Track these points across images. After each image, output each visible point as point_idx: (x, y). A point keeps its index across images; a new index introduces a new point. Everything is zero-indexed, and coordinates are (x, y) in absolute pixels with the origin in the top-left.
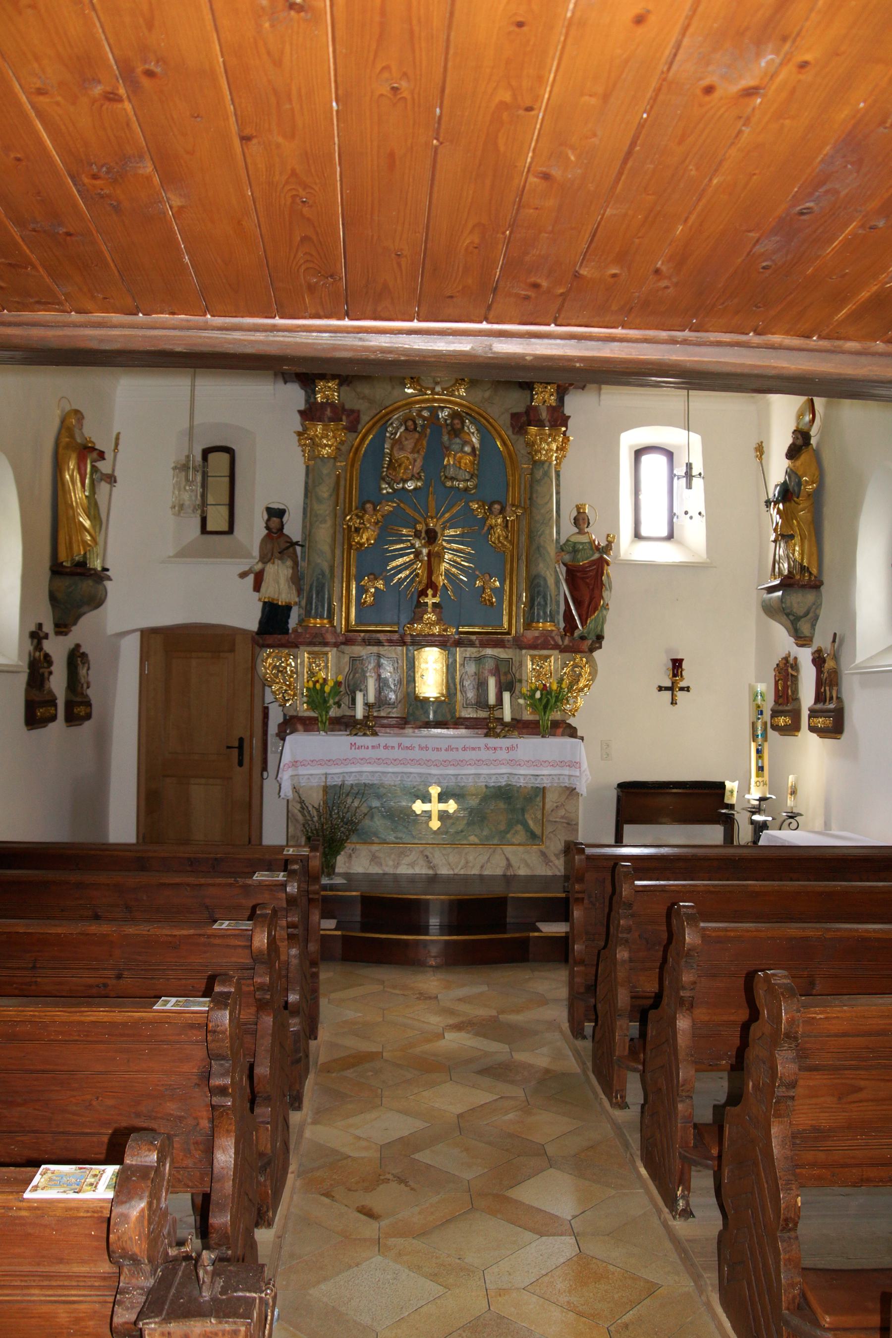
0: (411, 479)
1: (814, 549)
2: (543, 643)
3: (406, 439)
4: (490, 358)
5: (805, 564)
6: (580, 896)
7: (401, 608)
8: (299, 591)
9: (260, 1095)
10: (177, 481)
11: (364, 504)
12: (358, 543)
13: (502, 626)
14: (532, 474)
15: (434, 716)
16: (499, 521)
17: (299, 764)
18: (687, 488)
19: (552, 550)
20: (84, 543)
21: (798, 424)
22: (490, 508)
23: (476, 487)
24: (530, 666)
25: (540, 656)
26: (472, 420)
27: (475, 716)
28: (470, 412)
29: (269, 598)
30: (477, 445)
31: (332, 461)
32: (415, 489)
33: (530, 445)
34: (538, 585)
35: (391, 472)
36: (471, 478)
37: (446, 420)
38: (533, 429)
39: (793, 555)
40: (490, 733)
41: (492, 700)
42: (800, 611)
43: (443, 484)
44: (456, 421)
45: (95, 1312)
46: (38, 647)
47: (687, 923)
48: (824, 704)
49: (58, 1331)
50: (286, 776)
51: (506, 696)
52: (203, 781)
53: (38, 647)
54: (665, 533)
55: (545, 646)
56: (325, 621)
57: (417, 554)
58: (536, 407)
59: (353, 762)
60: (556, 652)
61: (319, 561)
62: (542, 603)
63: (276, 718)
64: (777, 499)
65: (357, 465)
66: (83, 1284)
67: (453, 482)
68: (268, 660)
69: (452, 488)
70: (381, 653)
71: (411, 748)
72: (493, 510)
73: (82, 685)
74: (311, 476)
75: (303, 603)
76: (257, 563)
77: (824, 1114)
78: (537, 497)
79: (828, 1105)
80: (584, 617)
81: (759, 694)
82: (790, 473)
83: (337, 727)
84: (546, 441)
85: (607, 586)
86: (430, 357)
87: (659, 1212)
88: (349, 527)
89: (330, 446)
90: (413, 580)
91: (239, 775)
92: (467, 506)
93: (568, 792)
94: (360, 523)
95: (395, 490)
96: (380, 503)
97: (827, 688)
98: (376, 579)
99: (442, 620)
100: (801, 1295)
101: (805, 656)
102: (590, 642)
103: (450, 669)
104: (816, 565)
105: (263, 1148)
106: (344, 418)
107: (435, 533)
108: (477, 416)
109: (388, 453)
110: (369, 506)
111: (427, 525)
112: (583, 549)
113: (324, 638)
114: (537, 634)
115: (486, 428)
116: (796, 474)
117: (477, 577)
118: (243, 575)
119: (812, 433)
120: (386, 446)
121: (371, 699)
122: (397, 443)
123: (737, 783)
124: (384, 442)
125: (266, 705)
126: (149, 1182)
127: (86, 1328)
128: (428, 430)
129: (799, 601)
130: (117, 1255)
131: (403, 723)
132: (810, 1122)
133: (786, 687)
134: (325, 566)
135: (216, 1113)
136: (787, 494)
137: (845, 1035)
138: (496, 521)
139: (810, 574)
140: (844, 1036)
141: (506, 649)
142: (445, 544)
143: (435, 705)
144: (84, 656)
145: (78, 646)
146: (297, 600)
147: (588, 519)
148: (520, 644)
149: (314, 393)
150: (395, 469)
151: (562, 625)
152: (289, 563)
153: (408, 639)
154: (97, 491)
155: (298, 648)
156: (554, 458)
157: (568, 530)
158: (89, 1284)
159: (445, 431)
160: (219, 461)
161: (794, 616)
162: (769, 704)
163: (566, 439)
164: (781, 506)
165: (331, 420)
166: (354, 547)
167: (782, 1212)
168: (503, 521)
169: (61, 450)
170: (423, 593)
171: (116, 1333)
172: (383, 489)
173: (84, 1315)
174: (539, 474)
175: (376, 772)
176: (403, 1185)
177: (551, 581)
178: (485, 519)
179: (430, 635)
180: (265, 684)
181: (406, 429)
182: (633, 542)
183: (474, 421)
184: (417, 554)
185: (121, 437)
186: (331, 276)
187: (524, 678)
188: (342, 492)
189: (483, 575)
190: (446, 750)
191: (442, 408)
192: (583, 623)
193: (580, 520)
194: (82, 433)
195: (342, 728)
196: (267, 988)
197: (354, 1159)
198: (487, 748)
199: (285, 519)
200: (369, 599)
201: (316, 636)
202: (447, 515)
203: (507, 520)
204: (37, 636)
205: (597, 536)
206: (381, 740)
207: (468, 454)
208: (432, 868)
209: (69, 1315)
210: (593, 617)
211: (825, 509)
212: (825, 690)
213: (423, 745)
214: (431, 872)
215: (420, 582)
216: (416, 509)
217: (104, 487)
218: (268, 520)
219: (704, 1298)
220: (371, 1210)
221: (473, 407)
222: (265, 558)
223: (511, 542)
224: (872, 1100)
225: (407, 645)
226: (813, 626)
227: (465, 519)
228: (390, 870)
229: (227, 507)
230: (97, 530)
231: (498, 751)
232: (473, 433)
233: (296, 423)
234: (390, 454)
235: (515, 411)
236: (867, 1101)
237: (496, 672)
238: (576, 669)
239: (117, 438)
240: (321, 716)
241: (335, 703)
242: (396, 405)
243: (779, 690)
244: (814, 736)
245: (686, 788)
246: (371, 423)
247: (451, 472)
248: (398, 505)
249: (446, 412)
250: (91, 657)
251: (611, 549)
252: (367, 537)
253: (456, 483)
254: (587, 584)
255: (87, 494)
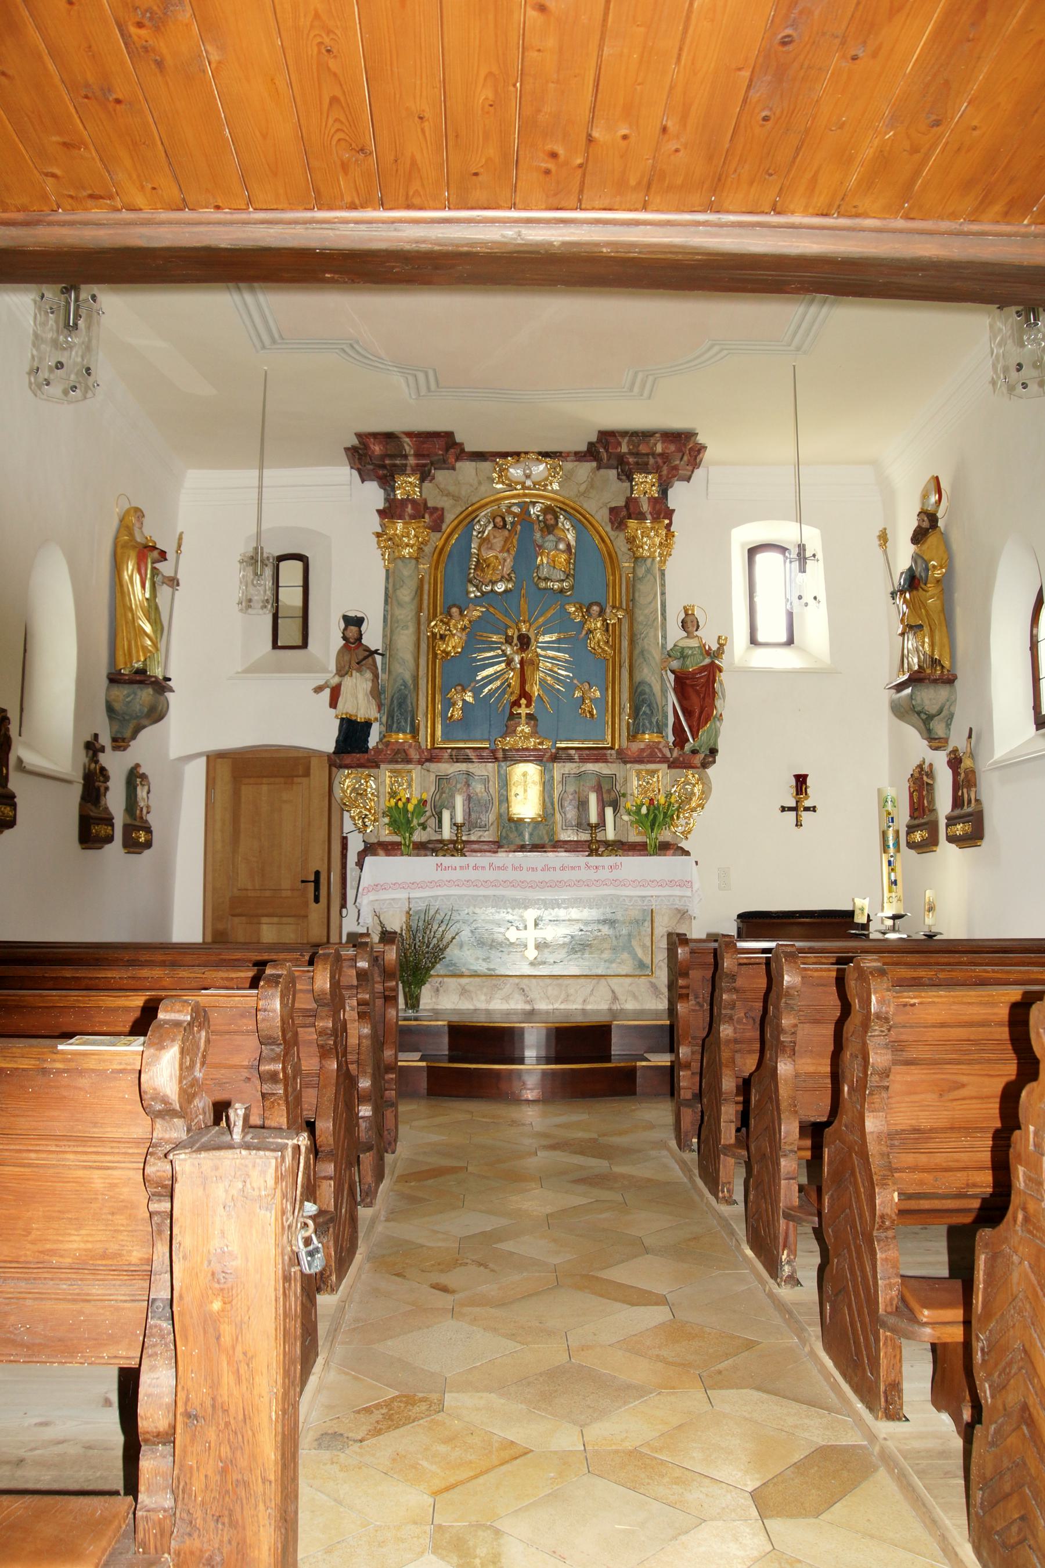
0: (501, 580)
1: (946, 641)
2: (649, 756)
3: (495, 537)
4: (520, 245)
5: (936, 657)
6: (684, 991)
7: (492, 722)
8: (380, 706)
9: (322, 1149)
10: (243, 576)
11: (450, 608)
12: (444, 651)
13: (604, 740)
14: (634, 572)
15: (530, 839)
16: (599, 625)
17: (379, 887)
18: (800, 571)
19: (656, 655)
20: (145, 648)
21: (923, 504)
22: (588, 611)
23: (572, 588)
24: (635, 783)
25: (647, 771)
26: (568, 516)
27: (575, 839)
28: (564, 507)
29: (346, 714)
30: (573, 543)
31: (414, 562)
32: (506, 591)
33: (631, 540)
34: (643, 693)
35: (479, 573)
36: (567, 578)
37: (538, 516)
38: (632, 523)
39: (923, 647)
40: (594, 852)
41: (594, 819)
42: (933, 709)
43: (537, 585)
44: (549, 517)
45: (129, 1179)
46: (94, 759)
47: (786, 960)
48: (962, 809)
49: (93, 1196)
50: (365, 901)
51: (609, 811)
52: (275, 920)
53: (94, 759)
54: (784, 638)
55: (652, 758)
56: (409, 736)
57: (509, 662)
58: (636, 498)
59: (438, 884)
60: (665, 766)
61: (401, 670)
62: (648, 712)
63: (355, 845)
64: (903, 586)
65: (441, 566)
66: (117, 1151)
67: (546, 583)
68: (346, 781)
69: (545, 589)
70: (470, 770)
71: (504, 868)
72: (592, 611)
73: (142, 809)
74: (391, 580)
75: (384, 719)
76: (334, 676)
77: (923, 1113)
78: (639, 597)
79: (927, 1103)
80: (695, 730)
81: (889, 800)
82: (916, 558)
83: (423, 852)
84: (648, 536)
85: (720, 694)
86: (463, 246)
87: (763, 1282)
88: (434, 635)
89: (412, 546)
90: (504, 692)
91: (316, 912)
92: (563, 607)
93: (679, 916)
94: (445, 630)
95: (483, 594)
96: (467, 608)
97: (965, 790)
98: (464, 690)
99: (537, 733)
100: (900, 1297)
101: (940, 761)
102: (703, 756)
103: (547, 786)
104: (948, 657)
105: (325, 1206)
106: (427, 516)
107: (529, 638)
108: (572, 511)
109: (475, 553)
110: (454, 610)
111: (519, 630)
112: (693, 655)
113: (407, 755)
114: (642, 745)
115: (583, 524)
116: (923, 559)
117: (576, 687)
118: (318, 690)
119: (939, 515)
120: (473, 546)
121: (459, 819)
122: (484, 541)
123: (868, 899)
124: (470, 541)
125: (345, 835)
126: (182, 1029)
127: (121, 1194)
128: (519, 527)
129: (930, 697)
130: (149, 1096)
131: (497, 846)
132: (909, 1122)
133: (921, 798)
134: (408, 676)
135: (267, 1103)
136: (913, 581)
137: (943, 1025)
138: (595, 624)
139: (943, 667)
140: (942, 1027)
141: (609, 764)
142: (539, 650)
143: (531, 826)
144: (144, 777)
145: (138, 766)
146: (378, 716)
147: (698, 622)
148: (623, 757)
149: (394, 490)
150: (483, 570)
151: (671, 739)
152: (369, 675)
153: (500, 755)
154: (158, 594)
155: (379, 768)
156: (657, 554)
157: (675, 634)
158: (124, 1151)
159: (536, 527)
160: (291, 571)
161: (926, 714)
162: (903, 817)
163: (669, 534)
164: (908, 595)
165: (413, 517)
166: (439, 657)
167: (877, 1207)
168: (603, 625)
169: (119, 551)
170: (516, 703)
171: (149, 1181)
172: (471, 592)
173: (118, 1181)
174: (641, 571)
175: (465, 895)
176: (482, 1268)
177: (657, 688)
178: (583, 623)
179: (524, 749)
180: (343, 808)
181: (495, 526)
182: (748, 648)
183: (569, 516)
184: (509, 662)
185: (184, 536)
186: (362, 150)
187: (629, 792)
188: (426, 597)
189: (582, 684)
190: (543, 870)
191: (534, 504)
192: (695, 735)
193: (689, 623)
194: (142, 532)
195: (429, 853)
196: (329, 1032)
197: (429, 1248)
198: (587, 866)
199: (363, 628)
200: (457, 713)
201: (398, 752)
202: (541, 620)
203: (608, 624)
204: (93, 748)
205: (708, 637)
206: (471, 860)
207: (563, 552)
208: (529, 1002)
209: (102, 1181)
210: (706, 728)
211: (956, 595)
212: (963, 793)
213: (517, 865)
214: (528, 1007)
215: (512, 693)
216: (507, 613)
217: (164, 591)
218: (345, 629)
219: (807, 1349)
220: (446, 1286)
221: (567, 502)
222: (342, 671)
223: (613, 647)
224: (976, 1098)
225: (499, 761)
226: (948, 726)
227: (562, 623)
228: (482, 1006)
229: (301, 619)
230: (159, 636)
231: (601, 870)
232: (568, 530)
233: (375, 523)
234: (478, 555)
235: (613, 505)
236: (971, 1098)
237: (599, 789)
238: (687, 787)
239: (180, 539)
240: (405, 839)
241: (419, 825)
242: (483, 502)
243: (914, 803)
244: (953, 847)
245: (814, 917)
246: (456, 522)
247: (545, 572)
248: (488, 610)
249: (538, 507)
250: (150, 778)
251: (723, 653)
252: (454, 644)
253: (550, 584)
254: (698, 693)
255: (147, 595)
